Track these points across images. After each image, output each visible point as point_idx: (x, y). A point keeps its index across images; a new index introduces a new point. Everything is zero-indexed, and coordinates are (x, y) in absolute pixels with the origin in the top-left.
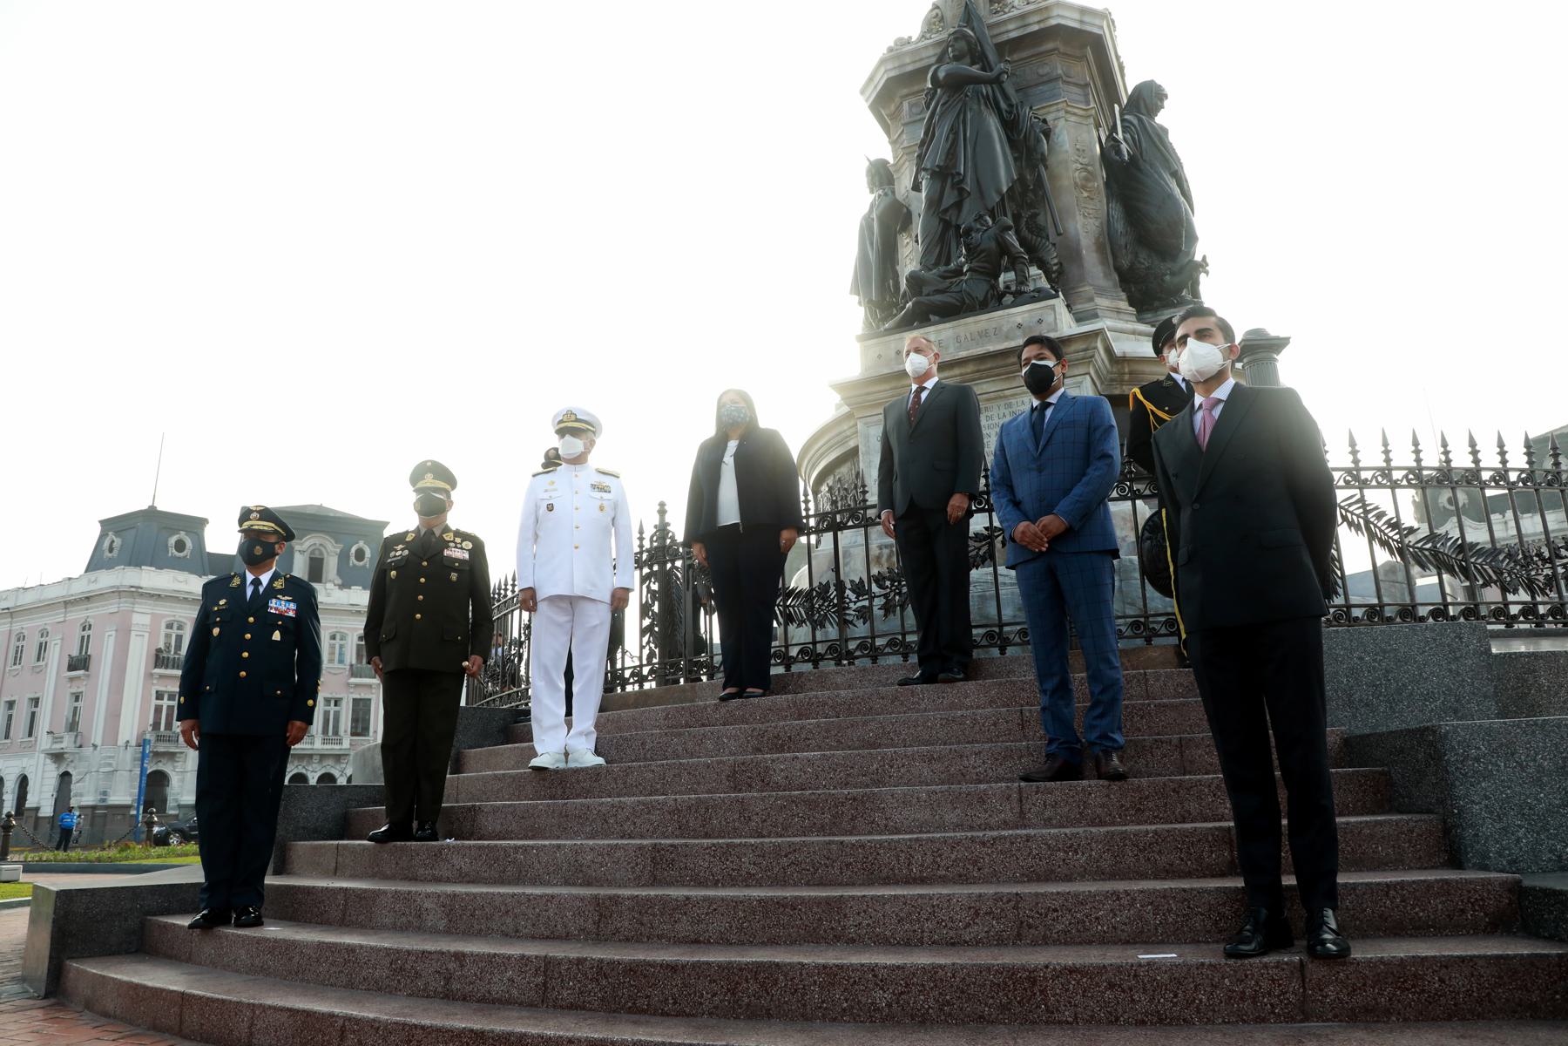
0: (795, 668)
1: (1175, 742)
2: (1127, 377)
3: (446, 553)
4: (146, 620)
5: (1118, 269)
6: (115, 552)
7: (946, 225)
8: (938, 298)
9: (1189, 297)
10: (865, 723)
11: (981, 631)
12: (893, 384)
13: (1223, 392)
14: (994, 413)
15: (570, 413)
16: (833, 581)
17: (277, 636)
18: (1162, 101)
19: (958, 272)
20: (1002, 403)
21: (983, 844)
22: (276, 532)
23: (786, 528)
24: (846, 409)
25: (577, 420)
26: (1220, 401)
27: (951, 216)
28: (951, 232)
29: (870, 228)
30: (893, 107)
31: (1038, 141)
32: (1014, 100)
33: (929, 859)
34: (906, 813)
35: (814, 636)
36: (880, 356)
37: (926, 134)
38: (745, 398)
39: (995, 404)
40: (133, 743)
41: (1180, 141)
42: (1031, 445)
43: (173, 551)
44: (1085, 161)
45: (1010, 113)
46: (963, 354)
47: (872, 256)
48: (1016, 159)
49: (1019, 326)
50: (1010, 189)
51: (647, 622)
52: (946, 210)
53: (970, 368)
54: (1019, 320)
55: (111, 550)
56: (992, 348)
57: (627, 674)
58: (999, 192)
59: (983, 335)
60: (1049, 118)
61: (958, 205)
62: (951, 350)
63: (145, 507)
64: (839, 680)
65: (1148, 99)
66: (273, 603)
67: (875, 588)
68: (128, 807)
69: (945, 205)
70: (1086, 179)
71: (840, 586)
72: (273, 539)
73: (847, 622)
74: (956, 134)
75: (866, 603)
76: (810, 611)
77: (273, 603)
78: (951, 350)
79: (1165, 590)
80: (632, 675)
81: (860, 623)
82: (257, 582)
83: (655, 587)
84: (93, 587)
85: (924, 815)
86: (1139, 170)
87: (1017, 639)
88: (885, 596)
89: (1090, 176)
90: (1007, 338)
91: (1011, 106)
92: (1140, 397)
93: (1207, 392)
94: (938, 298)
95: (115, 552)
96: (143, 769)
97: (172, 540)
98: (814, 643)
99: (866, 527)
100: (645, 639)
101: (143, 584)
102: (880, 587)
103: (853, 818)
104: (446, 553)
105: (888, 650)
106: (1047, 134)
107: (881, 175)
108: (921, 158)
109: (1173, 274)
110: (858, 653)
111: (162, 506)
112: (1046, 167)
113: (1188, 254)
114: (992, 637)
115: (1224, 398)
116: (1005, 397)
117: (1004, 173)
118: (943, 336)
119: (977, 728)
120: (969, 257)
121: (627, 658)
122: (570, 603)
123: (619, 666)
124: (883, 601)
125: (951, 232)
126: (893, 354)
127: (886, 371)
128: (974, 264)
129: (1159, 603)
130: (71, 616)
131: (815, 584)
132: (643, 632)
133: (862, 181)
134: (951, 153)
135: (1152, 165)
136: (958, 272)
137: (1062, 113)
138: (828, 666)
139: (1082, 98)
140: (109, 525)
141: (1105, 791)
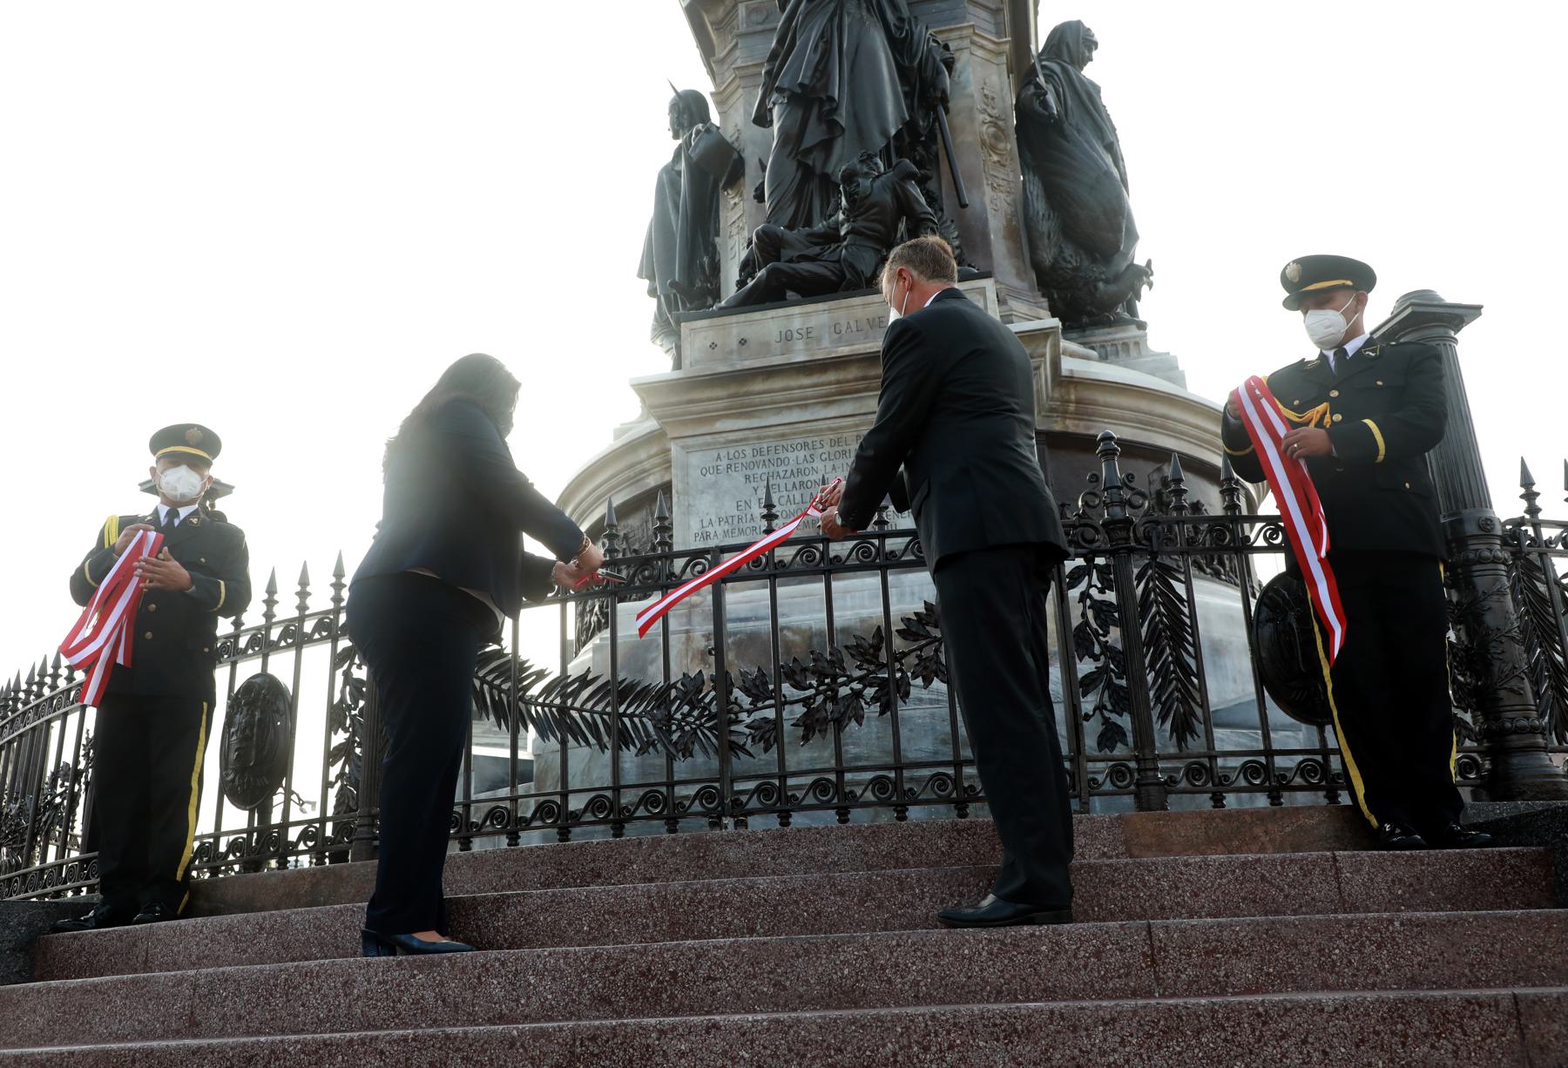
0: (578, 836)
1: (1506, 1004)
2: (1072, 407)
5: (1036, 266)
7: (807, 172)
9: (1126, 315)
10: (834, 948)
11: (691, 790)
12: (733, 390)
16: (709, 672)
18: (1090, 51)
19: (831, 237)
24: (652, 424)
27: (815, 160)
28: (814, 185)
29: (674, 185)
30: (721, 12)
31: (939, 72)
32: (906, 13)
35: (670, 770)
36: (713, 346)
37: (781, 42)
38: (1091, 44)
41: (1113, 102)
44: (995, 112)
45: (900, 29)
46: (844, 350)
47: (677, 223)
48: (906, 94)
50: (899, 133)
51: (340, 738)
52: (809, 151)
53: (853, 372)
57: (293, 834)
58: (884, 132)
60: (952, 46)
61: (826, 146)
62: (826, 343)
64: (732, 854)
65: (1073, 44)
67: (787, 688)
69: (808, 142)
70: (996, 137)
71: (723, 681)
73: (735, 748)
74: (829, 43)
75: (770, 714)
76: (664, 725)
78: (826, 343)
79: (1307, 709)
80: (304, 836)
83: (361, 673)
86: (1064, 136)
87: (869, 796)
88: (805, 701)
89: (1000, 134)
91: (901, 20)
98: (617, 788)
99: (773, 577)
100: (335, 770)
102: (797, 686)
105: (589, 817)
106: (950, 63)
107: (688, 110)
108: (772, 76)
109: (1107, 282)
112: (947, 111)
113: (1125, 255)
114: (883, 789)
117: (892, 109)
118: (813, 321)
119: (1062, 962)
120: (851, 213)
121: (294, 808)
123: (276, 818)
124: (800, 710)
125: (814, 185)
126: (734, 344)
128: (860, 223)
129: (1293, 735)
131: (675, 676)
132: (331, 756)
133: (663, 120)
134: (822, 69)
135: (1079, 131)
136: (831, 237)
137: (966, 43)
138: (694, 827)
139: (991, 27)
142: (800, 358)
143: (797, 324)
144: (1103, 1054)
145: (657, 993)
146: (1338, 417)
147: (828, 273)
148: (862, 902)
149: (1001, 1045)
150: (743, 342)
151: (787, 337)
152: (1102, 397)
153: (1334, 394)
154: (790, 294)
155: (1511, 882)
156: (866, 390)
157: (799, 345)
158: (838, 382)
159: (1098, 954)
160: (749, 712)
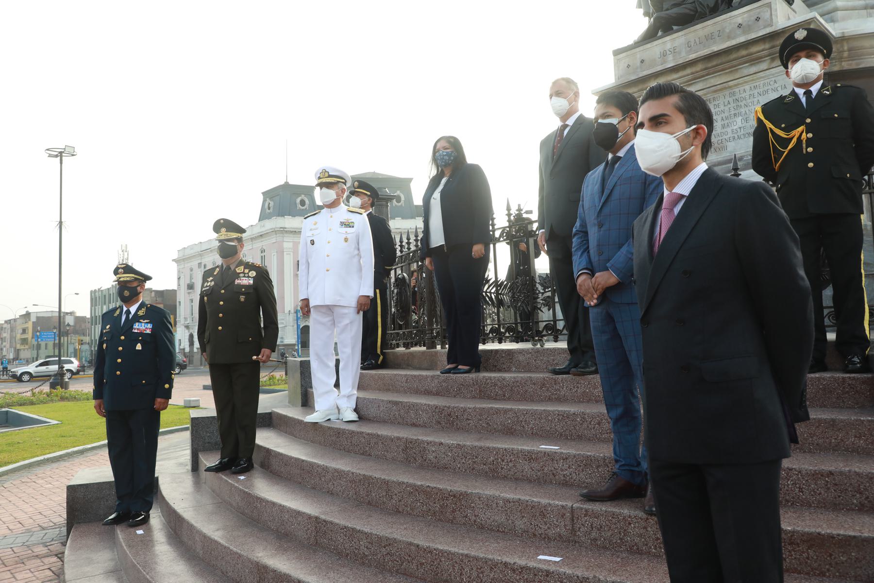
2: (846, 54)
3: (237, 282)
4: (290, 245)
6: (271, 210)
8: (675, 10)
13: (685, 186)
14: (721, 101)
15: (324, 171)
17: (139, 347)
20: (727, 92)
21: (514, 570)
22: (136, 279)
23: (477, 243)
25: (330, 176)
26: (682, 196)
33: (475, 574)
34: (488, 514)
36: (628, 66)
39: (721, 94)
40: (292, 311)
42: (597, 200)
43: (299, 206)
46: (693, 56)
49: (740, 26)
54: (740, 20)
55: (269, 208)
56: (716, 48)
59: (710, 37)
62: (683, 54)
63: (282, 183)
66: (136, 326)
68: (294, 345)
72: (135, 284)
77: (136, 326)
78: (683, 54)
81: (545, 309)
82: (128, 312)
84: (263, 229)
85: (501, 518)
90: (729, 38)
92: (762, 118)
93: (672, 186)
94: (675, 10)
95: (271, 210)
96: (298, 326)
97: (298, 200)
101: (286, 226)
103: (454, 511)
104: (237, 282)
110: (545, 333)
111: (292, 182)
115: (686, 192)
116: (730, 87)
118: (677, 43)
119: (585, 425)
122: (329, 309)
126: (639, 63)
127: (633, 77)
130: (255, 246)
140: (267, 195)
141: (643, 524)
142: (670, 65)
143: (669, 46)
144: (562, 470)
145: (453, 422)
146: (810, 135)
147: (687, 11)
148: (541, 388)
149: (527, 463)
150: (642, 61)
151: (664, 55)
152: (866, 43)
153: (808, 120)
154: (675, 28)
155: (848, 392)
156: (707, 75)
157: (670, 58)
158: (692, 73)
159: (599, 424)
160: (543, 293)
